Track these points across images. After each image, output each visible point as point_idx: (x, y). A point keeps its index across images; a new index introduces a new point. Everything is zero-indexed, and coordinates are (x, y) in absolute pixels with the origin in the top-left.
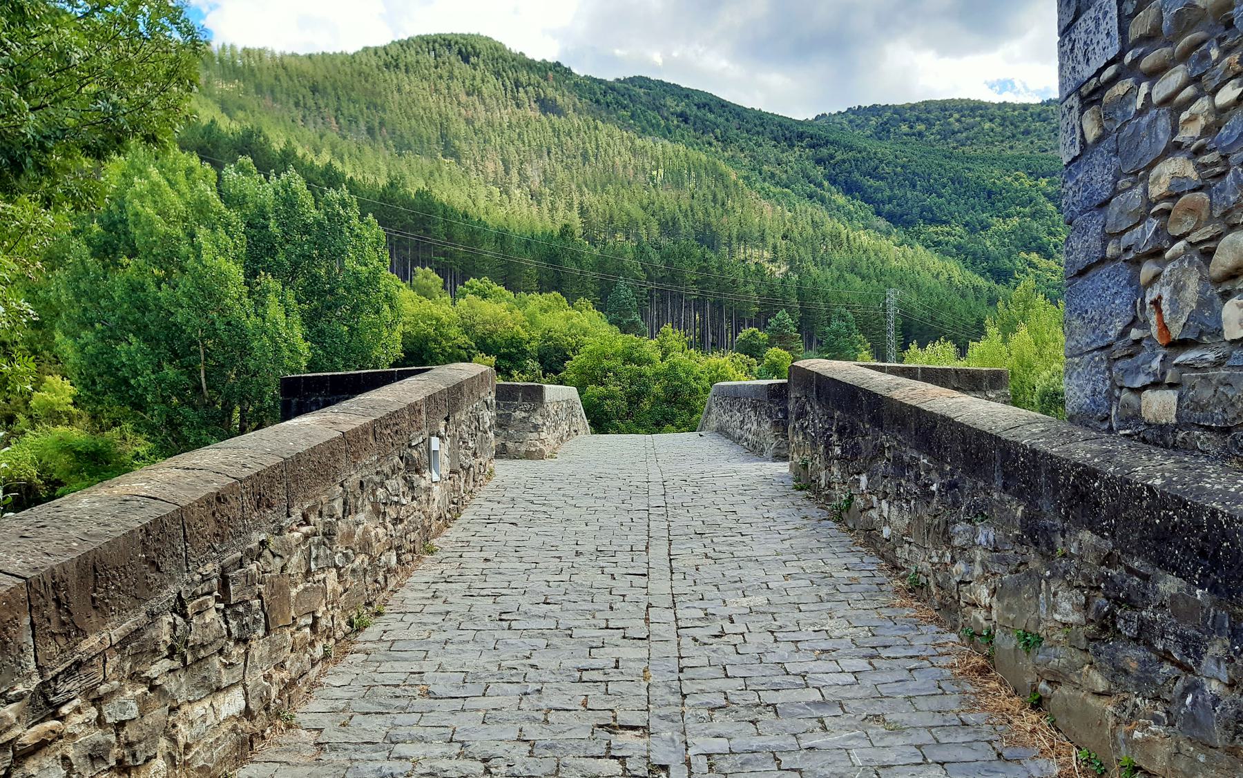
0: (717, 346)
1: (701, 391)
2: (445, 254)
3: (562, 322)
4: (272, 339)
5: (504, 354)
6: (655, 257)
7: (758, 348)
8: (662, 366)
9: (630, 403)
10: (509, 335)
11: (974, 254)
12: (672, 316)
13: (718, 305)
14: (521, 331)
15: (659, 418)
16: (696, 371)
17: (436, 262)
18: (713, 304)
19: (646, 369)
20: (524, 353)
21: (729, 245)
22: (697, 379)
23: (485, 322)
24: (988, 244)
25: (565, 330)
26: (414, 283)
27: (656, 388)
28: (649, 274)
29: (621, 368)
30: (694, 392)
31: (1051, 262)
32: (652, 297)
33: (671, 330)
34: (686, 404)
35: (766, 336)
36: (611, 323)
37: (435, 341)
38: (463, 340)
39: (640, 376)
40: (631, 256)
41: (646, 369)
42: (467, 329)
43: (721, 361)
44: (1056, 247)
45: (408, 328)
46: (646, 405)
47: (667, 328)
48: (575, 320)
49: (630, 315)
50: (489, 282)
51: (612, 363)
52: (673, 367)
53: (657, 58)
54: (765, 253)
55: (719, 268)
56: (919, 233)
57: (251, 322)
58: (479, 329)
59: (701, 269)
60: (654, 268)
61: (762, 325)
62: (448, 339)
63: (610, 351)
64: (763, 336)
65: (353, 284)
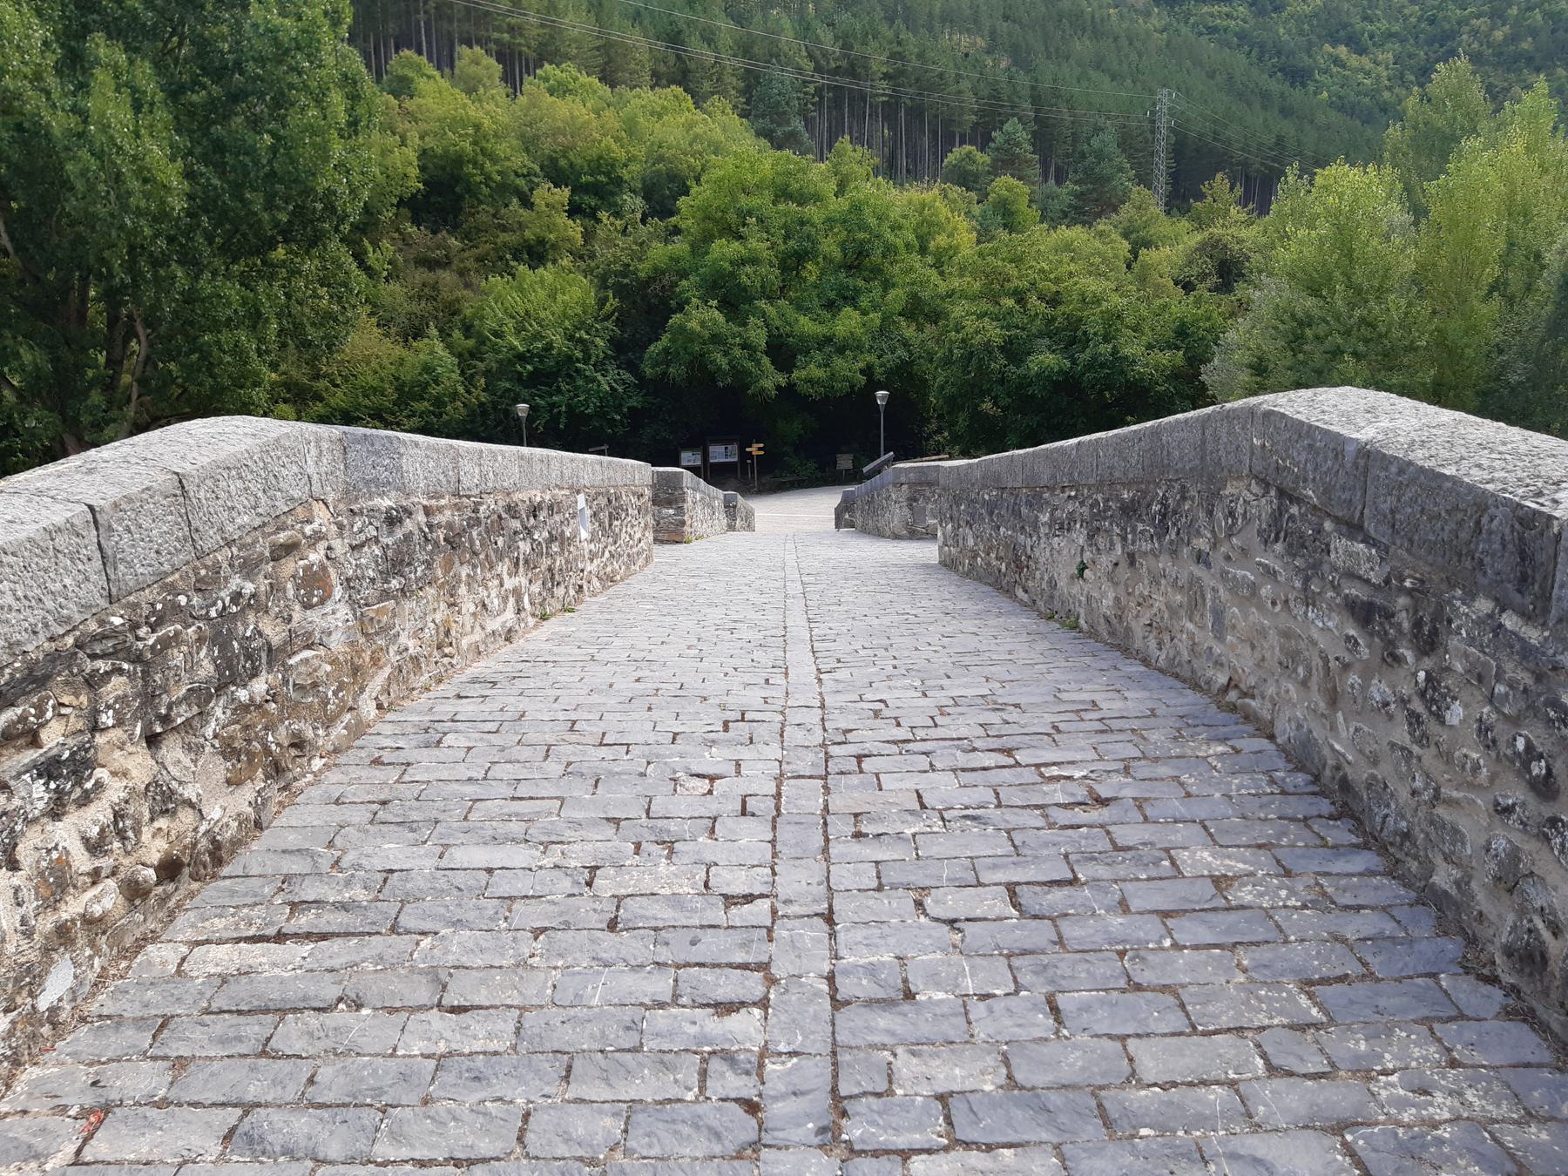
0: (914, 174)
1: (902, 249)
2: (512, 29)
3: (679, 132)
4: (99, 155)
5: (587, 184)
6: (826, 36)
7: (976, 176)
8: (838, 205)
9: (784, 268)
10: (594, 153)
11: (1262, 46)
12: (850, 128)
13: (916, 112)
14: (614, 147)
15: (832, 295)
16: (895, 214)
17: (497, 42)
18: (909, 111)
19: (812, 211)
20: (619, 182)
21: (930, 29)
22: (895, 227)
23: (556, 132)
24: (1282, 31)
25: (684, 144)
26: (457, 71)
27: (830, 246)
28: (817, 62)
29: (769, 210)
30: (890, 250)
31: (1365, 60)
32: (822, 98)
33: (850, 147)
34: (877, 271)
35: (987, 159)
36: (758, 134)
37: (475, 163)
38: (520, 161)
39: (802, 223)
40: (791, 33)
41: (812, 211)
42: (529, 144)
43: (928, 196)
44: (1371, 37)
45: (430, 142)
46: (811, 271)
47: (844, 143)
48: (698, 130)
49: (788, 124)
50: (575, 73)
51: (755, 201)
52: (856, 208)
53: (893, 550)
54: (979, 40)
55: (921, 56)
56: (1188, 15)
57: (58, 123)
58: (547, 146)
59: (893, 56)
60: (825, 55)
61: (984, 142)
62: (494, 159)
63: (751, 179)
64: (983, 159)
65: (269, 51)
